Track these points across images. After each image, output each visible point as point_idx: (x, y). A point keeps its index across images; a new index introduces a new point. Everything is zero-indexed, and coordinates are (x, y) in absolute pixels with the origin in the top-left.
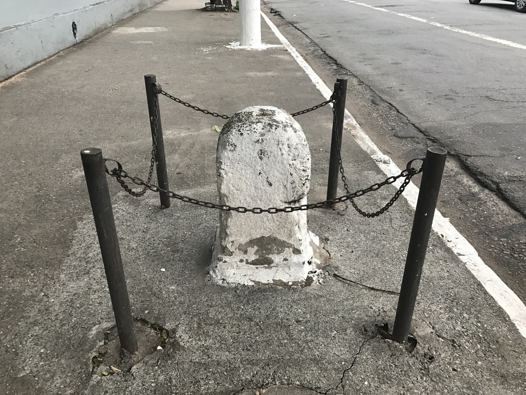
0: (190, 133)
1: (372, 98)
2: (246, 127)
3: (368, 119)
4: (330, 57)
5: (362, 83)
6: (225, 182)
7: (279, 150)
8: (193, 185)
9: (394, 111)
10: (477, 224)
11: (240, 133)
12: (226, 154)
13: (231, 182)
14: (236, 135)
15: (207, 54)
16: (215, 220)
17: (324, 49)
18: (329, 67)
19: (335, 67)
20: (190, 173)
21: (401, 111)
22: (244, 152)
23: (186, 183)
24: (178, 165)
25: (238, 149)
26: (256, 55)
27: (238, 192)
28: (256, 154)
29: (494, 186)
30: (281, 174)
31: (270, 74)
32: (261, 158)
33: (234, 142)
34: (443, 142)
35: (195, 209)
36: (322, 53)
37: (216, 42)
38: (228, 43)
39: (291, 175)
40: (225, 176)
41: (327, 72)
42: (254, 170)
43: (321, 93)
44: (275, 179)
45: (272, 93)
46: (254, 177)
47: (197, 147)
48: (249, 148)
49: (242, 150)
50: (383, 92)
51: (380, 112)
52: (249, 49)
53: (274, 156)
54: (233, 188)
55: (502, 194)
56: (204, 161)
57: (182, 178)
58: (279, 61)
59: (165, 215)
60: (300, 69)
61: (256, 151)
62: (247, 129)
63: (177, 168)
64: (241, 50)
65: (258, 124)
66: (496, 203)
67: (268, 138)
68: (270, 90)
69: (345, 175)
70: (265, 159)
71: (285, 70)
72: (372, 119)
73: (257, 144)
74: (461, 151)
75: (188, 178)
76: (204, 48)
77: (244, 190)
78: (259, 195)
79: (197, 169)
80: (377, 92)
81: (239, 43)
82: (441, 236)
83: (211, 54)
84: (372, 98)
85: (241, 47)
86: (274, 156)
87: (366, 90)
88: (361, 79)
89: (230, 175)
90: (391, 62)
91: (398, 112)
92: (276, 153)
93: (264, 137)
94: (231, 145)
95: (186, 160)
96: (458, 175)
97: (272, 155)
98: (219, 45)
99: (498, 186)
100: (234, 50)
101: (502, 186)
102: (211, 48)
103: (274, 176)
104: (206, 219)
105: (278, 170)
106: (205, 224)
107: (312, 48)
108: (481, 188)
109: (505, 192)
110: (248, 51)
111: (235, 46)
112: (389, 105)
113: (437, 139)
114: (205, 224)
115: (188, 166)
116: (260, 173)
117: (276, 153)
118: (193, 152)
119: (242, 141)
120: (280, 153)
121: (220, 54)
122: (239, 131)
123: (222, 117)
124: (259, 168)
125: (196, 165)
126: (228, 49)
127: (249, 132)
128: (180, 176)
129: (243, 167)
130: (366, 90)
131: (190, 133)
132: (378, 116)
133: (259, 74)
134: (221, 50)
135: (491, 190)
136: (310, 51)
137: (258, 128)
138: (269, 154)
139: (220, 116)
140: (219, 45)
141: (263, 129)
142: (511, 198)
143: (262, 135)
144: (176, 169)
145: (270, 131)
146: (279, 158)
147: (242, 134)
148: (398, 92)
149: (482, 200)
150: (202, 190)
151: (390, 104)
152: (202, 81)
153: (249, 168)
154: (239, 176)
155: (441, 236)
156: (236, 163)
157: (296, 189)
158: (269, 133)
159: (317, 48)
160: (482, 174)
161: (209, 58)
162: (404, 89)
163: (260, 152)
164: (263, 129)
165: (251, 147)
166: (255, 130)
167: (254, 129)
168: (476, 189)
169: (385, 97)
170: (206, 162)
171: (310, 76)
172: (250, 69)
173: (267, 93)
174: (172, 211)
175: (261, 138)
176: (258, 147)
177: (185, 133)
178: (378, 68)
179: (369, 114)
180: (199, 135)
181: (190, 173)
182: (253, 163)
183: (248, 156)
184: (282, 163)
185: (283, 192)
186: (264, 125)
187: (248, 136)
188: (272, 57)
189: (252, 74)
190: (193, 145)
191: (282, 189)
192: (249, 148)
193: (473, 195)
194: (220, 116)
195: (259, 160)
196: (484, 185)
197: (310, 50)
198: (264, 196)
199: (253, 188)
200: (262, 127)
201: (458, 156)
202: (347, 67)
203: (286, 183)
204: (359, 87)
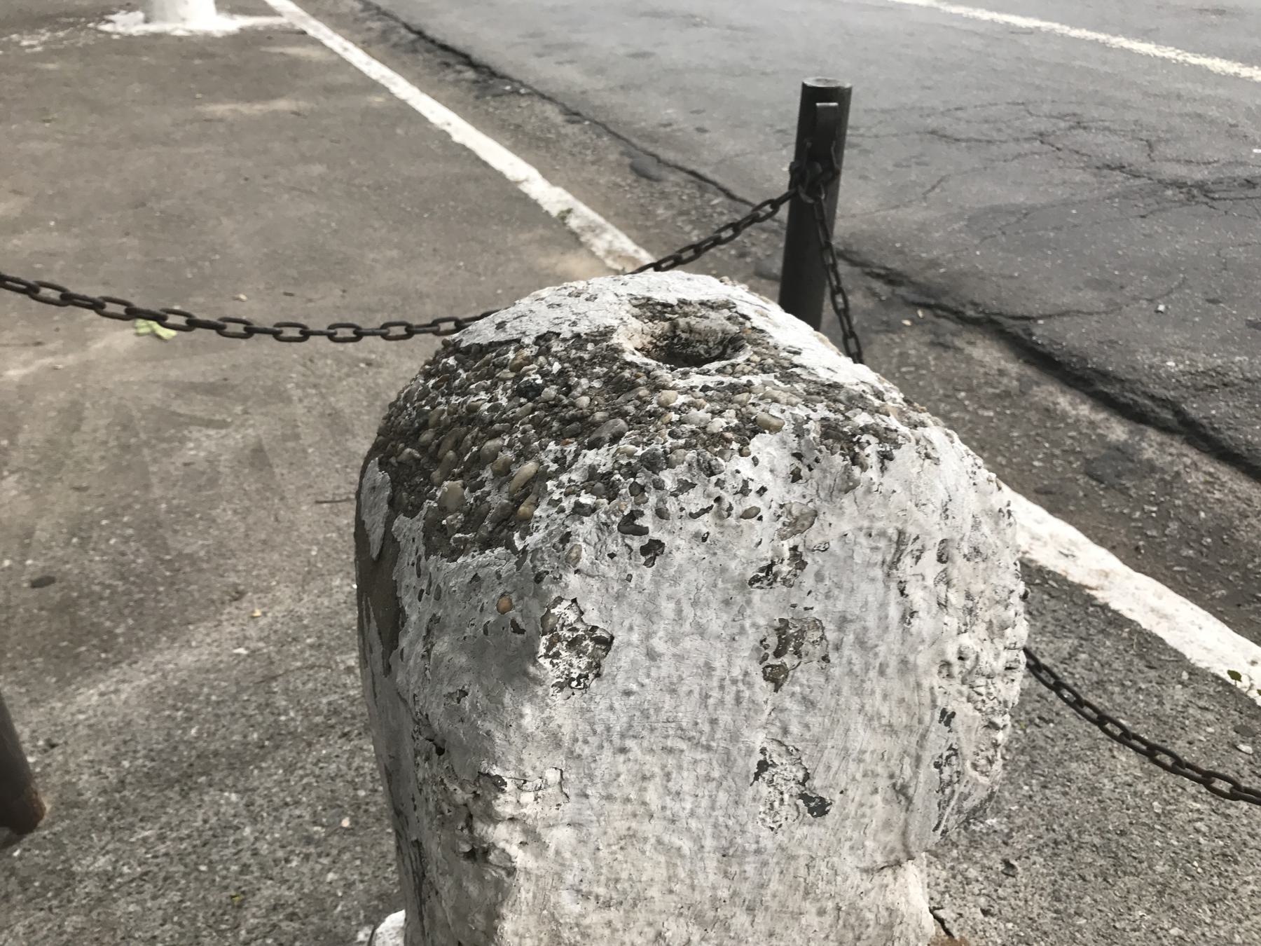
0: (48, 361)
1: (627, 161)
2: (685, 486)
3: (647, 228)
4: (445, 48)
5: (576, 118)
6: (525, 892)
7: (894, 592)
8: (132, 639)
9: (717, 195)
10: (1204, 565)
11: (637, 543)
12: (530, 717)
13: (570, 878)
14: (604, 567)
15: (35, 54)
16: (309, 840)
17: (414, 23)
18: (451, 76)
19: (470, 74)
20: (97, 565)
21: (739, 194)
22: (666, 668)
23: (95, 630)
24: (29, 534)
25: (621, 660)
26: (210, 49)
27: (612, 914)
28: (744, 661)
29: (1167, 415)
30: (891, 730)
31: (282, 105)
32: (776, 677)
33: (592, 617)
34: (920, 279)
35: (184, 795)
36: (412, 36)
37: (60, 15)
38: (103, 14)
39: (947, 718)
40: (521, 858)
41: (452, 90)
42: (727, 761)
43: (478, 158)
44: (852, 766)
45: (318, 169)
46: (722, 797)
47: (96, 422)
48: (701, 630)
49: (652, 655)
50: (652, 138)
51: (676, 201)
52: (179, 33)
53: (861, 643)
54: (577, 909)
55: (1206, 439)
56: (147, 487)
57: (65, 607)
58: (295, 63)
59: (24, 883)
60: (375, 87)
61: (748, 643)
62: (695, 500)
63: (25, 550)
64: (157, 36)
65: (756, 443)
66: (1210, 474)
67: (832, 536)
68: (305, 159)
69: (377, 321)
70: (805, 675)
71: (329, 90)
72: (657, 225)
73: (757, 594)
74: (994, 306)
75: (94, 599)
76: (20, 33)
77: (654, 892)
78: (745, 888)
79: (126, 540)
80: (634, 140)
81: (140, 15)
82: (1229, 679)
83: (51, 52)
84: (627, 161)
85: (153, 28)
86: (861, 643)
87: (599, 136)
88: (568, 104)
89: (560, 837)
90: (622, 51)
91: (729, 195)
92: (871, 621)
93: (814, 536)
94: (573, 644)
95: (63, 502)
96: (1030, 388)
97: (850, 638)
98: (72, 25)
99: (1178, 413)
100: (131, 36)
101: (1193, 409)
102: (46, 35)
103: (845, 754)
104: (264, 848)
105: (871, 719)
106: (268, 890)
107: (377, 25)
108: (1133, 426)
109: (1214, 429)
110: (180, 39)
111: (127, 24)
112: (692, 178)
113: (899, 274)
114: (268, 890)
115: (80, 531)
116: (763, 766)
117: (871, 621)
118: (82, 450)
119: (653, 598)
120: (894, 613)
121: (85, 51)
122: (630, 526)
123: (276, 335)
124: (759, 739)
125: (113, 514)
126: (108, 34)
127: (705, 524)
128: (54, 593)
129: (652, 764)
130: (599, 136)
131: (48, 361)
132: (674, 217)
133: (245, 108)
134: (83, 39)
135: (1164, 428)
136: (373, 35)
137: (766, 479)
138: (831, 635)
139: (264, 331)
140: (72, 25)
141: (796, 477)
142: (1243, 448)
143: (797, 523)
144: (25, 556)
145: (849, 486)
146: (888, 648)
147: (653, 550)
148: (697, 137)
149: (1163, 471)
150: (187, 658)
151: (693, 173)
152: (46, 146)
153: (688, 756)
154: (621, 826)
155: (1229, 679)
156: (606, 756)
157: (959, 788)
158: (847, 501)
159: (392, 23)
160: (1105, 376)
161: (51, 66)
162: (707, 124)
163: (773, 641)
164: (796, 477)
165: (715, 620)
166: (752, 501)
167: (744, 491)
168: (1118, 431)
169: (670, 155)
170: (157, 492)
171: (412, 103)
172: (212, 95)
173: (300, 170)
174: (60, 847)
175: (786, 545)
176: (765, 608)
177: (26, 364)
178: (601, 71)
179: (647, 213)
180: (87, 367)
181: (97, 565)
182: (725, 718)
183: (692, 683)
184: (905, 665)
185: (887, 825)
186: (793, 442)
187: (700, 551)
188: (271, 54)
189: (221, 109)
190: (73, 417)
191: (880, 807)
192: (701, 630)
193: (1121, 452)
194: (264, 331)
195: (762, 688)
196: (1134, 415)
197: (370, 29)
198: (774, 886)
199: (712, 863)
200: (785, 463)
201: (992, 322)
202: (508, 70)
203: (908, 772)
204: (571, 129)
